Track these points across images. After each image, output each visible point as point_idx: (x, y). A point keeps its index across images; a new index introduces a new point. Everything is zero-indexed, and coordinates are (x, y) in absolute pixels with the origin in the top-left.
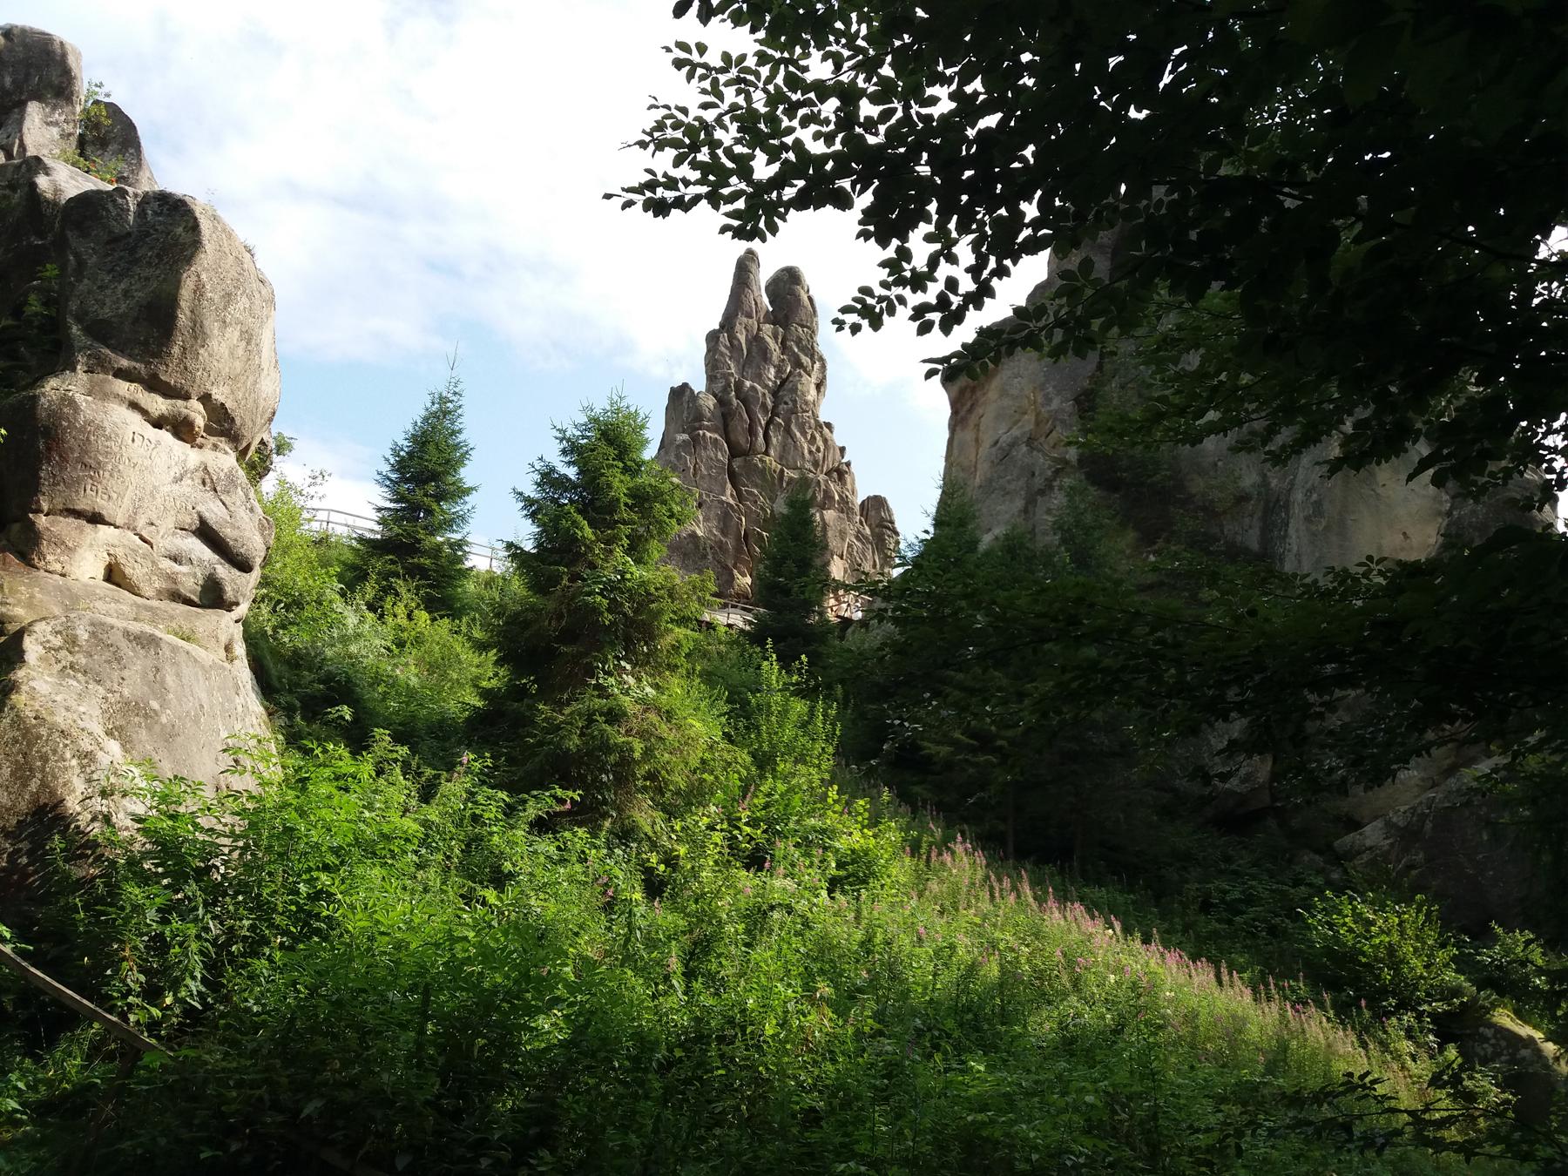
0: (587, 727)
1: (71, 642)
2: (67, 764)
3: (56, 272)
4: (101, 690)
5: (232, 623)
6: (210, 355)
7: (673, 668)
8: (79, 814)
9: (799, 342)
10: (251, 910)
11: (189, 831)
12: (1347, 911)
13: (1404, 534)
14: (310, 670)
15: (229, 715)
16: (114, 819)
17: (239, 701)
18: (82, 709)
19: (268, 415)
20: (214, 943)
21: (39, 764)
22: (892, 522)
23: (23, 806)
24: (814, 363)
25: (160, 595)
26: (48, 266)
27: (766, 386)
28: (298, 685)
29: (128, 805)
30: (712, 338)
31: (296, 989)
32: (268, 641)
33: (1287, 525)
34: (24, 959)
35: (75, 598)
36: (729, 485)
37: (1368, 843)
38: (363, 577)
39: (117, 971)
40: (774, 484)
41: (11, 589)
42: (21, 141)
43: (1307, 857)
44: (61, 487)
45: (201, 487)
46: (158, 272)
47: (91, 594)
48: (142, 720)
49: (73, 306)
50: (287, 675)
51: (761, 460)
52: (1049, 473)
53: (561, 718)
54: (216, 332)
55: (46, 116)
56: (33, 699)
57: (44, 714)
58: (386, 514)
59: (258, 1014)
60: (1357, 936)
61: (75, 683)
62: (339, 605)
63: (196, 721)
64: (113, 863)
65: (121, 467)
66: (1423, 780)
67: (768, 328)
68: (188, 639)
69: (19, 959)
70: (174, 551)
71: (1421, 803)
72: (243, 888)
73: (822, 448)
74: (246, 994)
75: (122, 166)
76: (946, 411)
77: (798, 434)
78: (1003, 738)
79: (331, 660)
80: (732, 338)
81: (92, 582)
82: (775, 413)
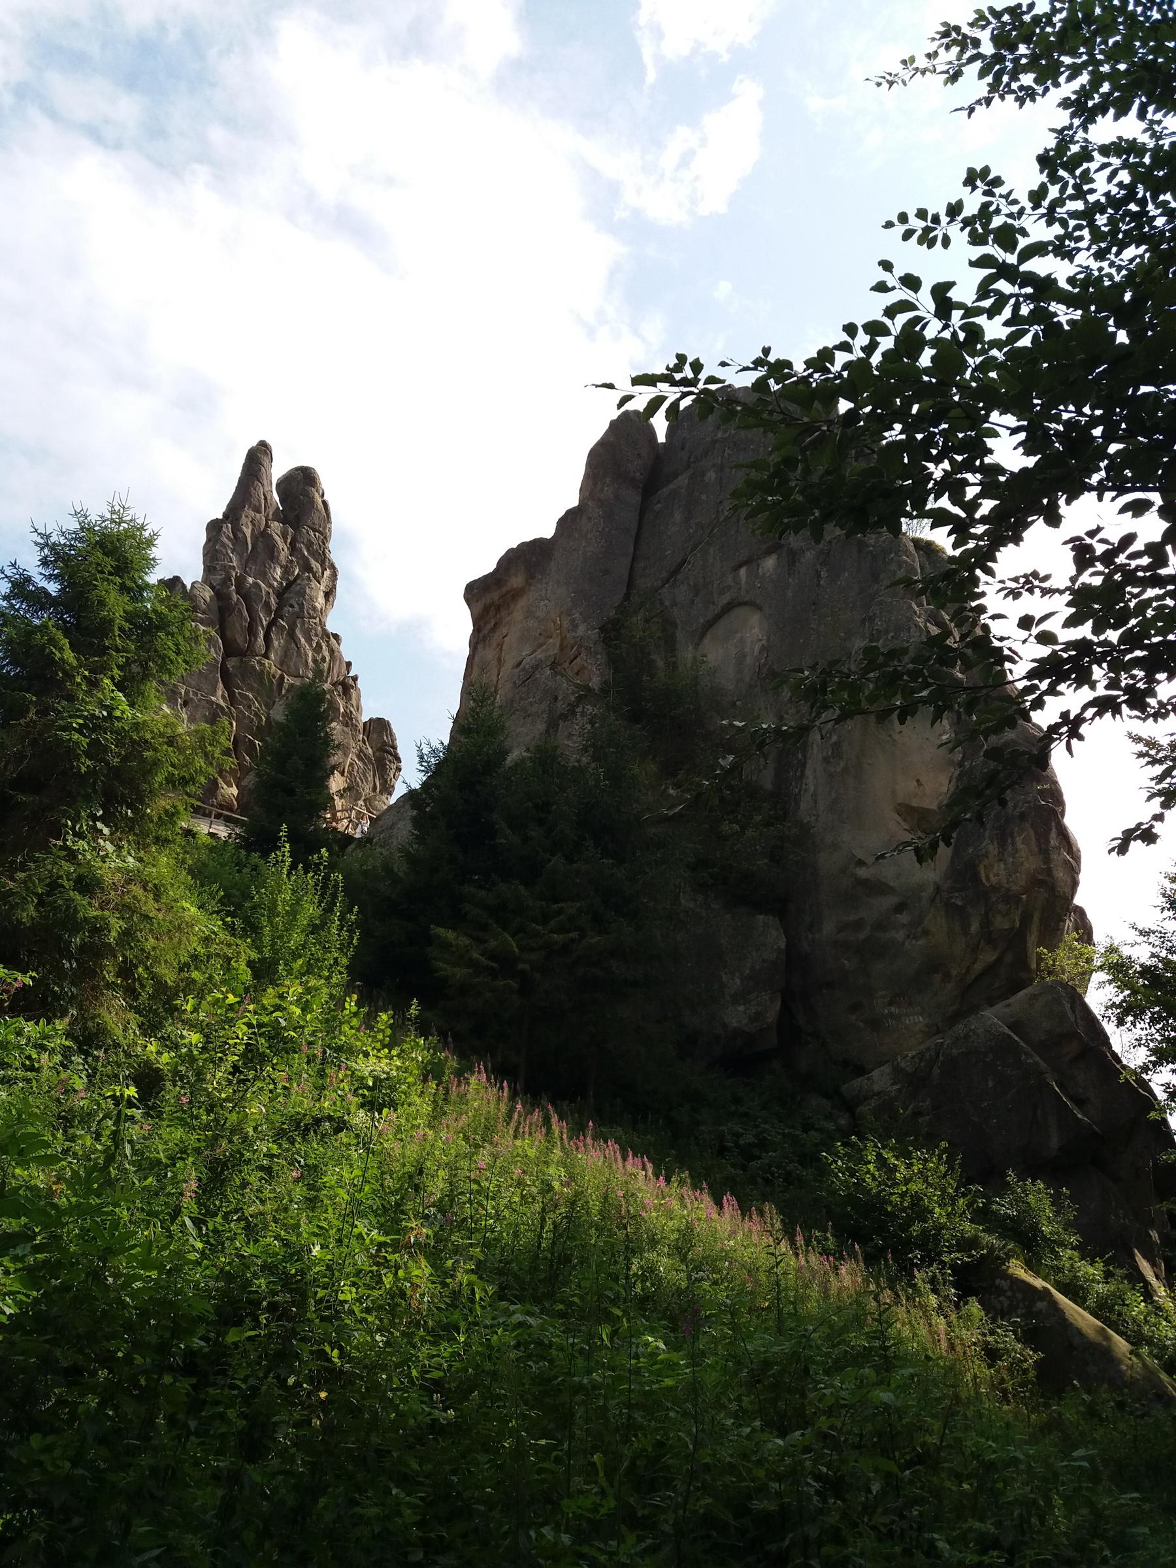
0: (48, 894)
7: (162, 842)
9: (309, 546)
12: (871, 1157)
13: (918, 781)
22: (395, 748)
24: (324, 569)
27: (271, 586)
30: (214, 527)
33: (804, 766)
36: (221, 686)
37: (876, 1088)
40: (271, 689)
51: (259, 662)
52: (573, 698)
53: (11, 885)
60: (880, 1184)
66: (927, 1026)
67: (276, 526)
71: (928, 1049)
73: (328, 659)
76: (468, 627)
77: (303, 640)
80: (236, 529)
82: (279, 614)
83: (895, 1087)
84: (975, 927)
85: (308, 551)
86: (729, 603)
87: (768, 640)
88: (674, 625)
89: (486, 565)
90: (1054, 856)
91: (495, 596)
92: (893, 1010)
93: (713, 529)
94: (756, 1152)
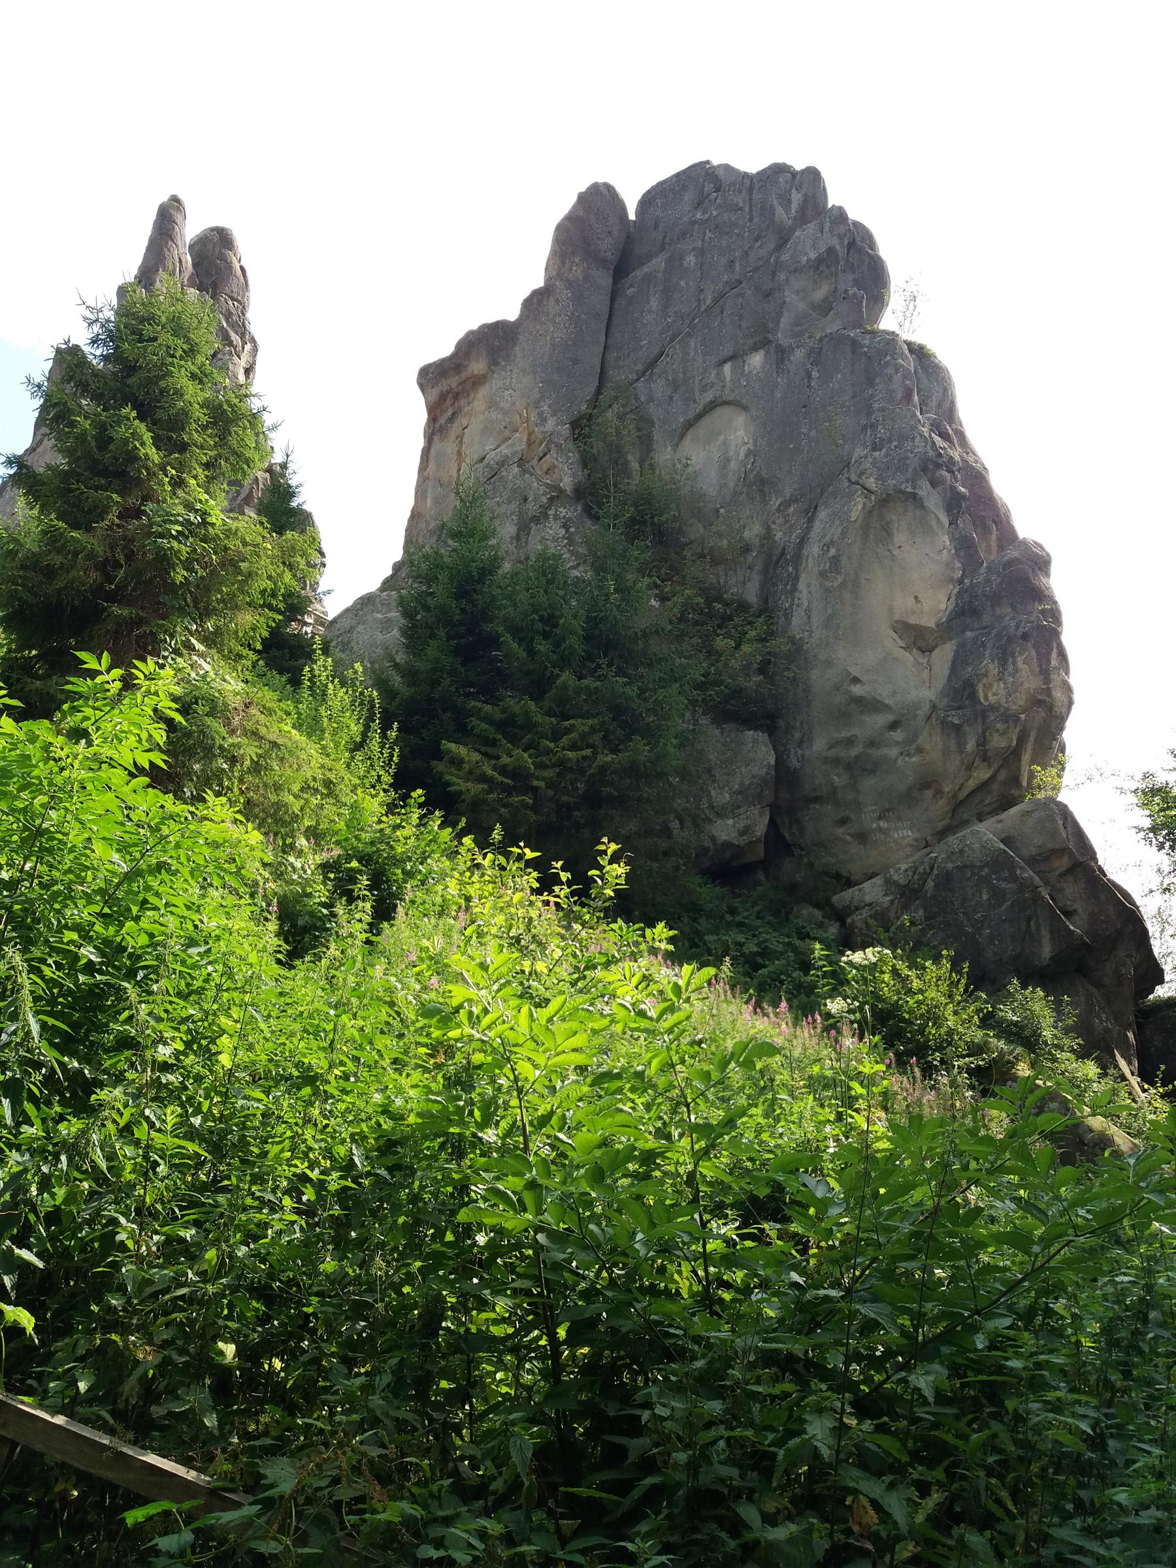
13: (916, 597)
33: (797, 579)
37: (868, 899)
43: (807, 911)
66: (916, 840)
76: (422, 416)
78: (537, 779)
83: (888, 898)
84: (971, 745)
85: (227, 321)
86: (711, 402)
87: (755, 444)
88: (651, 423)
89: (444, 348)
90: (1053, 676)
91: (453, 382)
92: (881, 824)
93: (694, 319)
94: (759, 960)
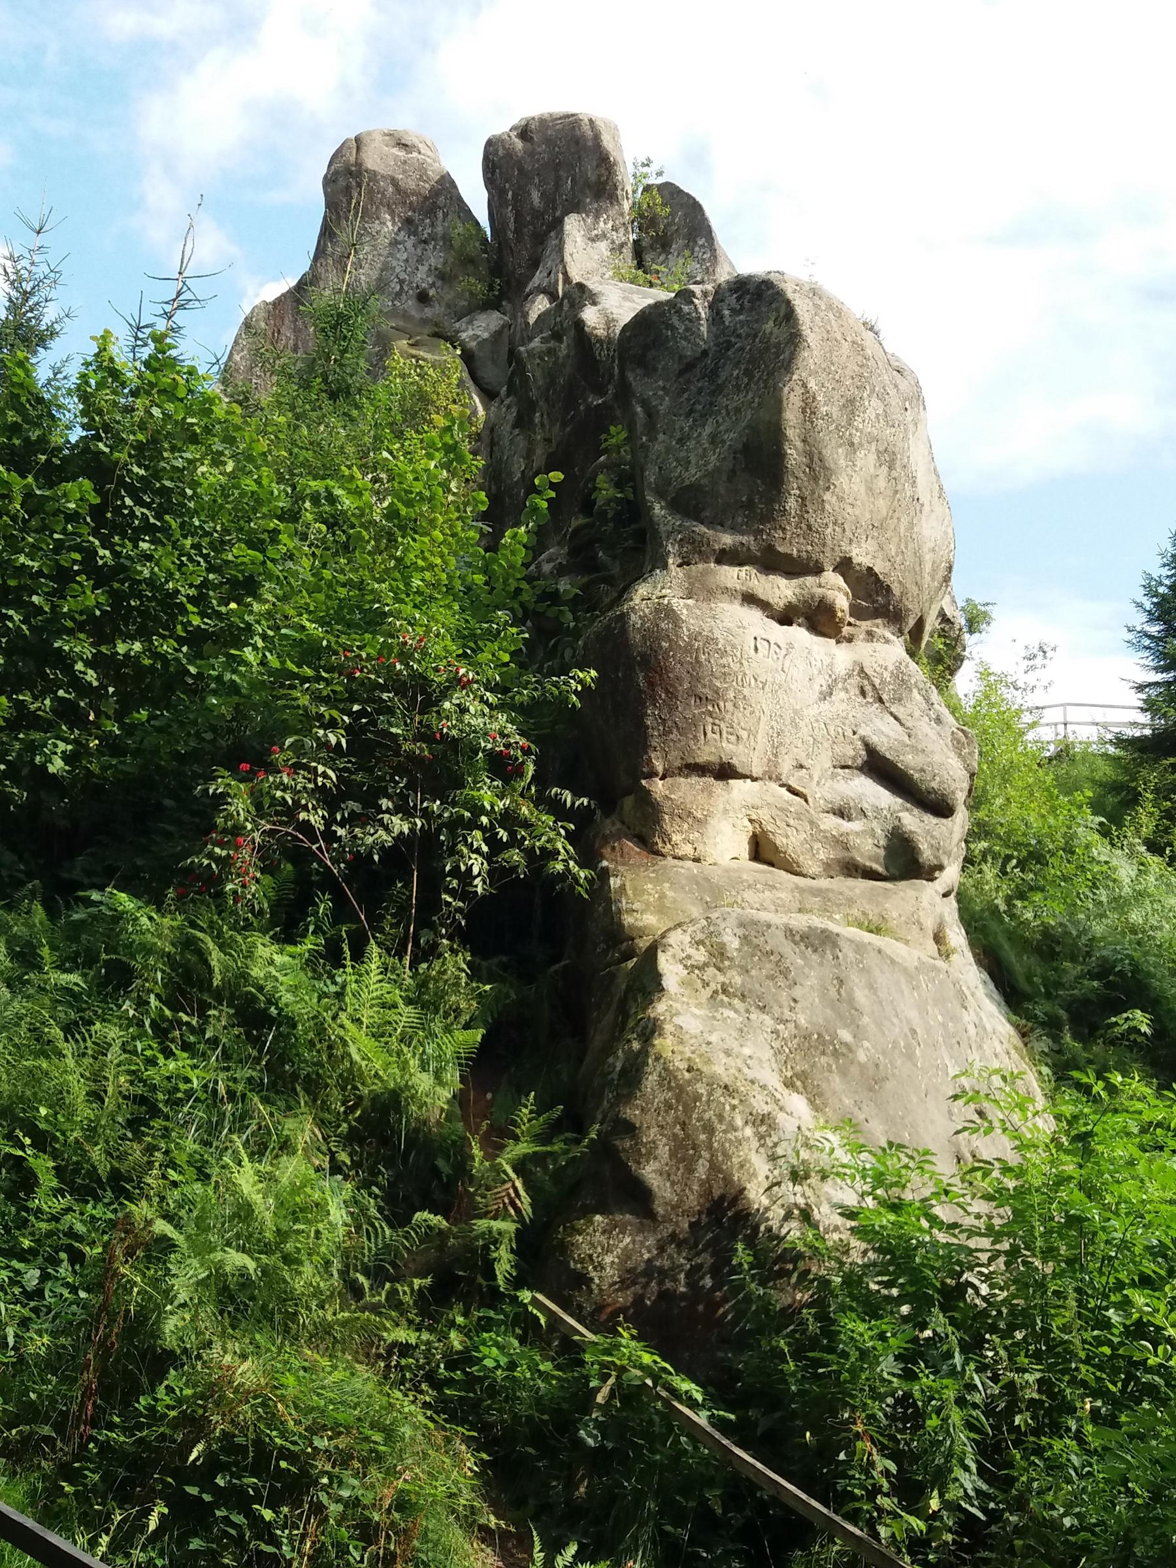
1: (719, 954)
2: (739, 1134)
3: (624, 435)
4: (767, 1020)
5: (938, 899)
6: (841, 499)
8: (767, 1209)
10: (1037, 1356)
11: (920, 1230)
14: (1073, 959)
15: (957, 1042)
16: (816, 1215)
17: (968, 1018)
18: (747, 1051)
19: (941, 573)
20: (989, 1411)
21: (703, 1137)
23: (693, 1201)
25: (829, 869)
26: (612, 429)
28: (1059, 985)
29: (831, 1192)
31: (1128, 1489)
32: (1002, 921)
34: (724, 1434)
35: (716, 892)
38: (1132, 800)
39: (851, 1454)
41: (635, 890)
42: (565, 274)
44: (675, 735)
45: (860, 699)
46: (750, 395)
47: (736, 883)
48: (831, 1060)
49: (651, 475)
50: (1039, 971)
54: (842, 463)
55: (589, 230)
56: (682, 1042)
57: (698, 1063)
58: (1153, 692)
59: (1072, 1531)
61: (732, 1014)
62: (1101, 850)
63: (910, 1056)
64: (825, 1283)
65: (746, 691)
68: (877, 931)
69: (717, 1435)
70: (838, 802)
72: (1019, 1319)
74: (1049, 1498)
75: (693, 266)
79: (1103, 938)
81: (734, 864)
